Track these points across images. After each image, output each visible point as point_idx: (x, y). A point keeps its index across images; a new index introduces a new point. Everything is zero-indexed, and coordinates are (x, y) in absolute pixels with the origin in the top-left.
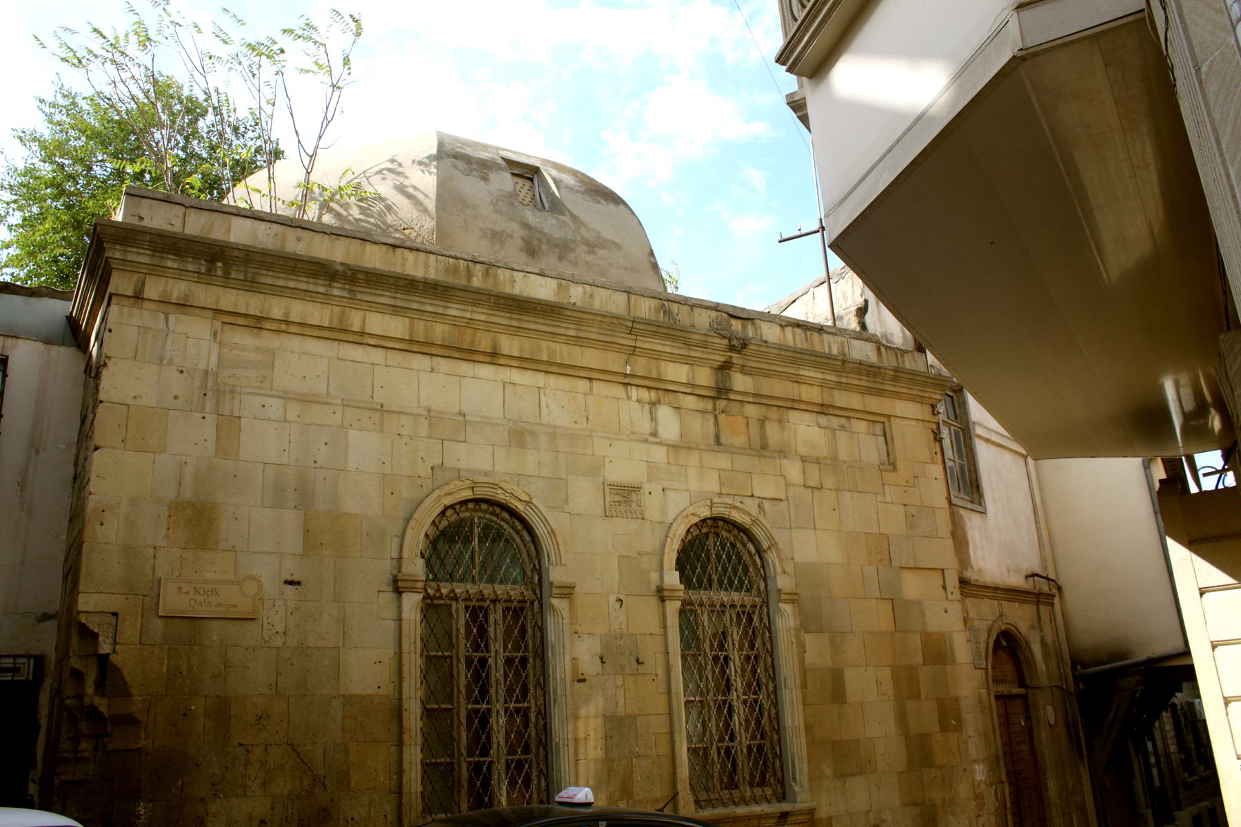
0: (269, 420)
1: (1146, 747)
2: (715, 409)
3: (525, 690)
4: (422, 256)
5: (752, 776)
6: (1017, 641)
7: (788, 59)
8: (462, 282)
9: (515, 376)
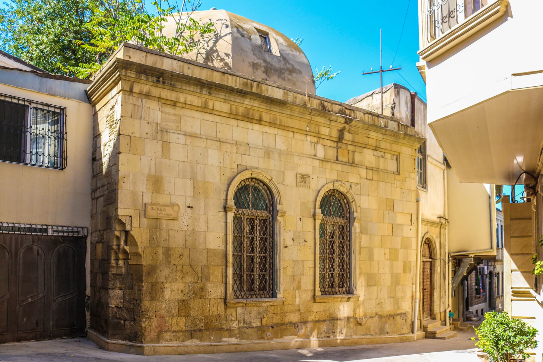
0: (180, 144)
1: (465, 283)
4: (234, 77)
5: (339, 284)
6: (431, 242)
8: (249, 90)
9: (266, 129)
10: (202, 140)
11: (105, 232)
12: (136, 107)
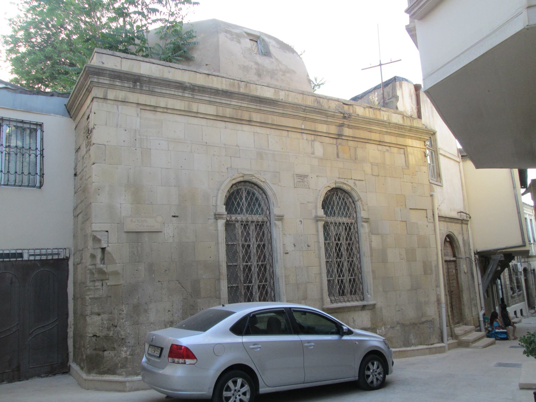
1: (497, 282)
4: (220, 78)
9: (258, 130)
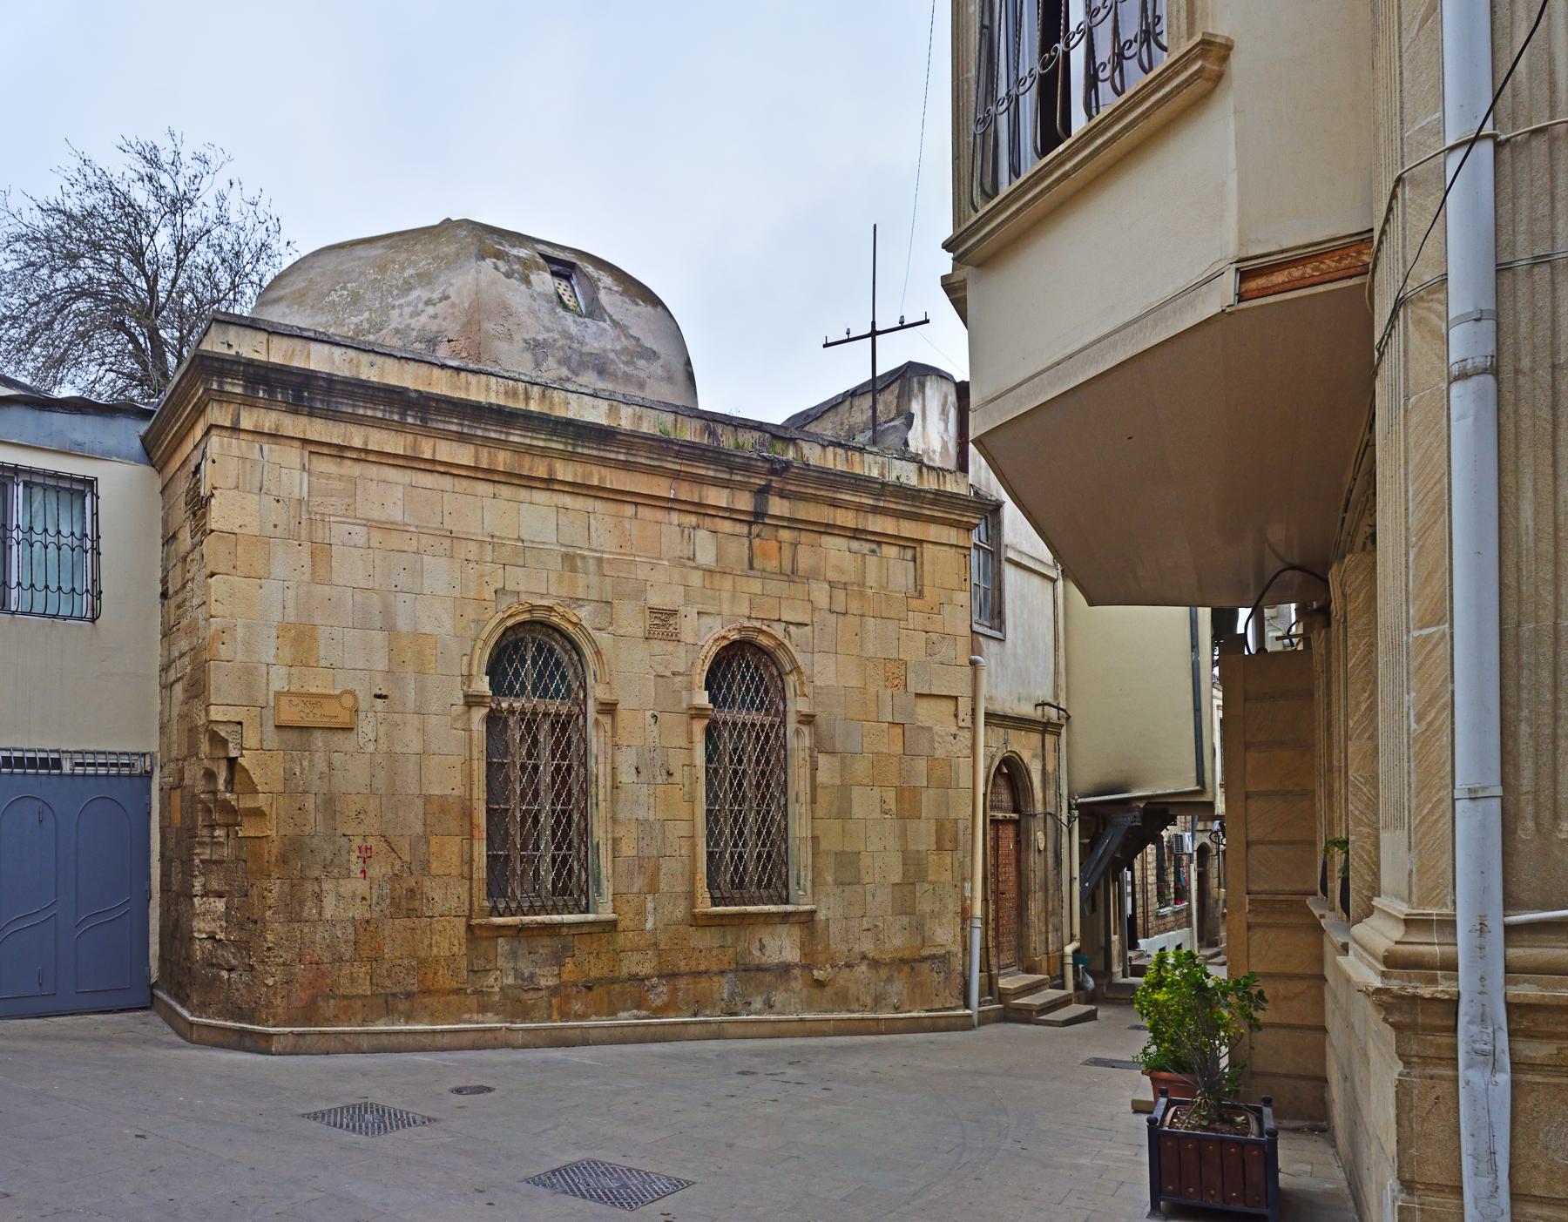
0: (355, 546)
2: (750, 533)
3: (536, 794)
4: (483, 377)
5: (760, 880)
7: (958, 247)
8: (521, 406)
9: (567, 500)
10: (407, 535)
11: (186, 763)
12: (248, 464)
